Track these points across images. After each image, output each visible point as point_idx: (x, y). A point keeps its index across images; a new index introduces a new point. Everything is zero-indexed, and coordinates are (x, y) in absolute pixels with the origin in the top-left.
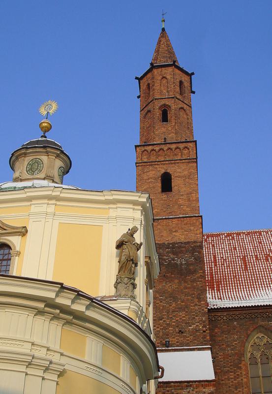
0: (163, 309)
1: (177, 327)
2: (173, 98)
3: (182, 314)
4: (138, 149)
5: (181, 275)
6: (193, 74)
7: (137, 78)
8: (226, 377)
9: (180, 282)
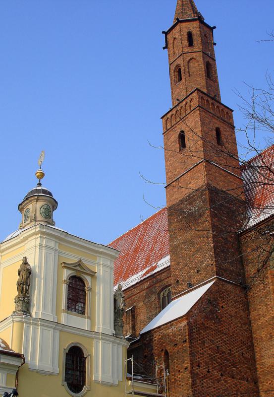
7: (163, 32)
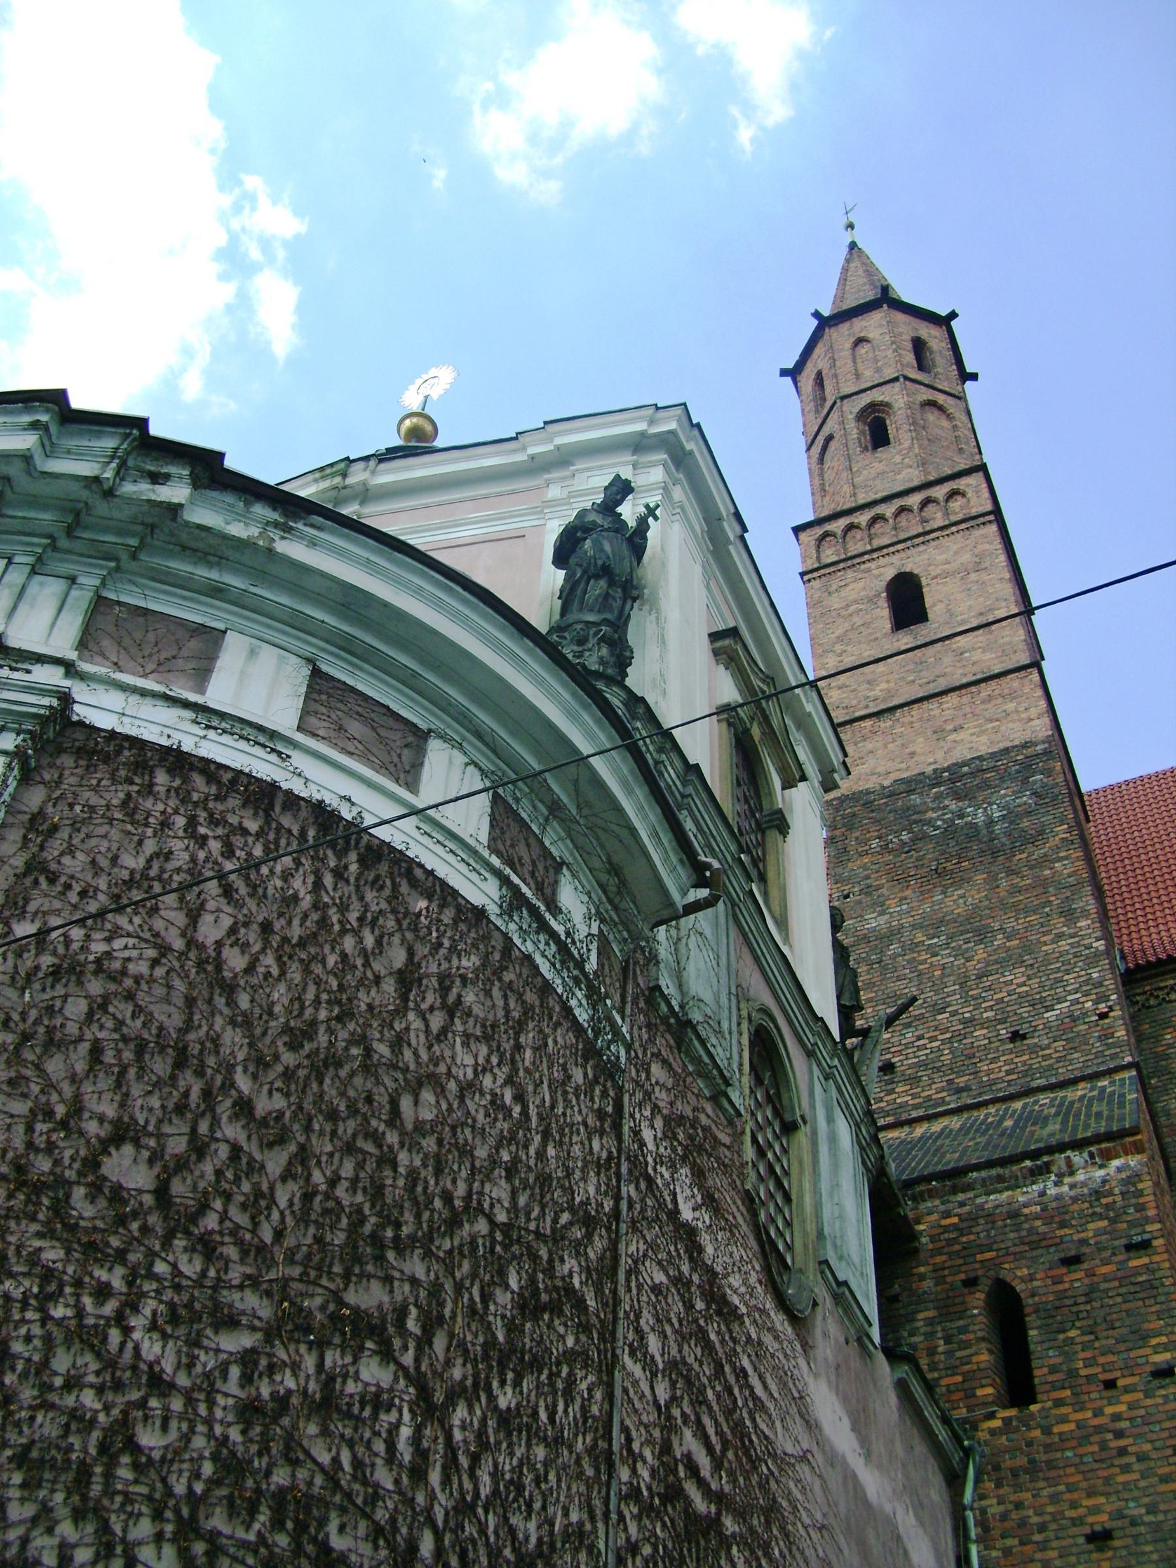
0: (943, 975)
1: (1003, 1021)
2: (896, 379)
3: (1016, 976)
4: (803, 536)
5: (994, 854)
6: (953, 315)
8: (1122, 1408)
9: (992, 879)
